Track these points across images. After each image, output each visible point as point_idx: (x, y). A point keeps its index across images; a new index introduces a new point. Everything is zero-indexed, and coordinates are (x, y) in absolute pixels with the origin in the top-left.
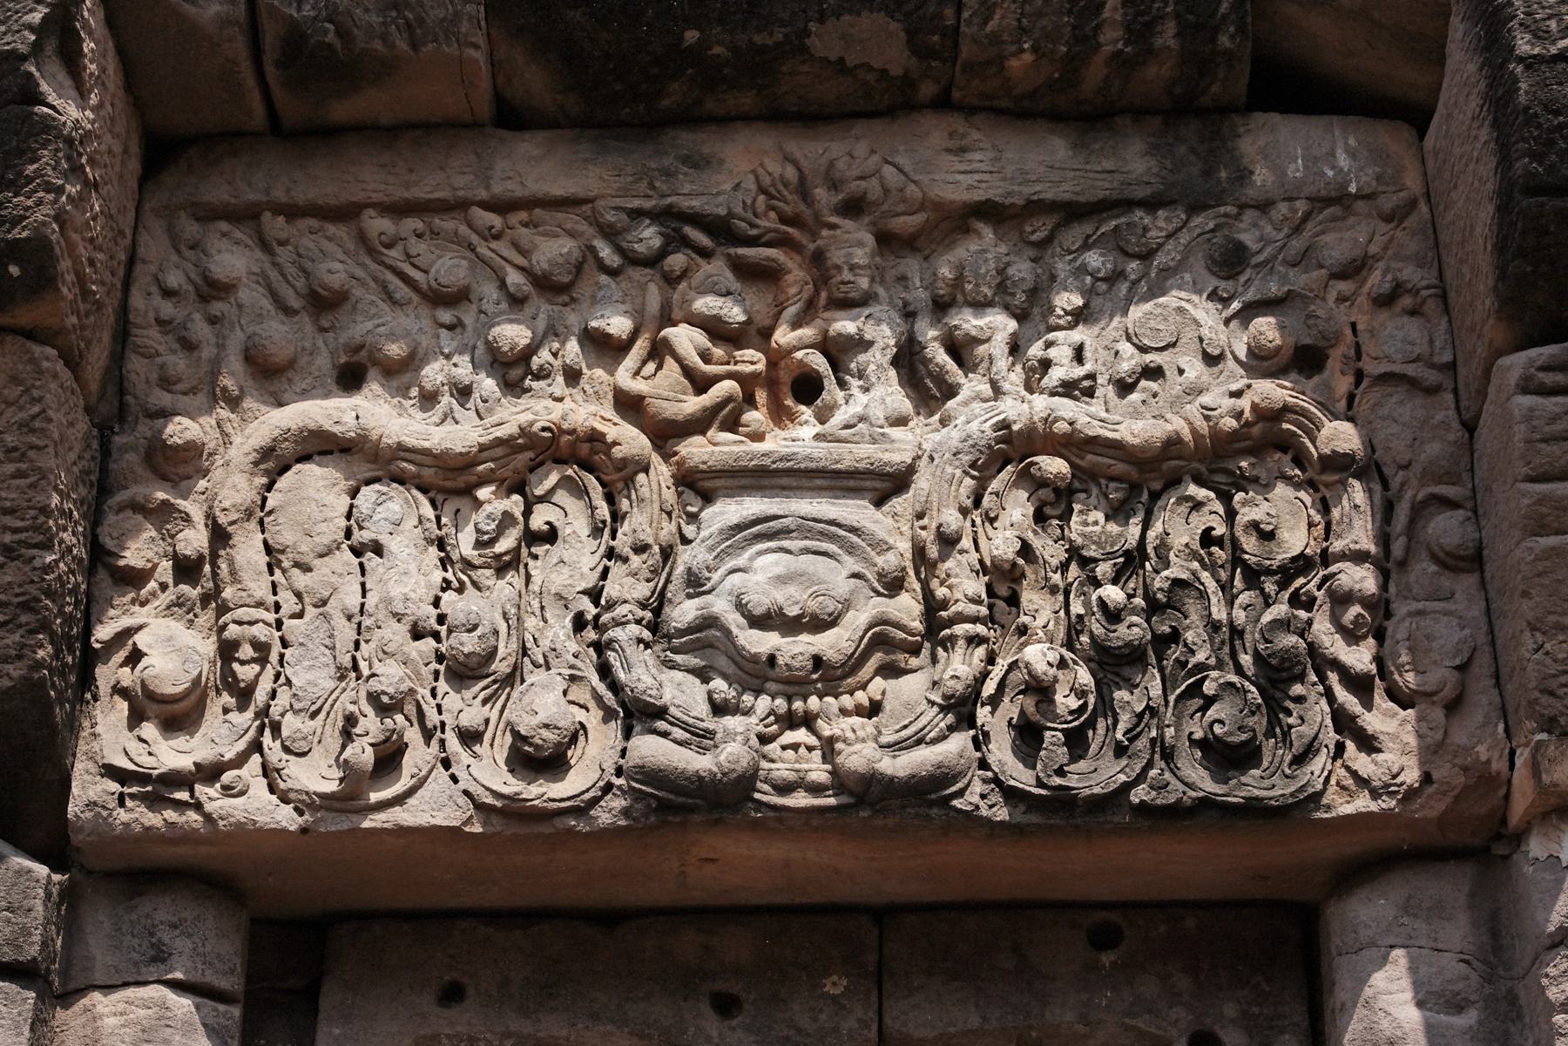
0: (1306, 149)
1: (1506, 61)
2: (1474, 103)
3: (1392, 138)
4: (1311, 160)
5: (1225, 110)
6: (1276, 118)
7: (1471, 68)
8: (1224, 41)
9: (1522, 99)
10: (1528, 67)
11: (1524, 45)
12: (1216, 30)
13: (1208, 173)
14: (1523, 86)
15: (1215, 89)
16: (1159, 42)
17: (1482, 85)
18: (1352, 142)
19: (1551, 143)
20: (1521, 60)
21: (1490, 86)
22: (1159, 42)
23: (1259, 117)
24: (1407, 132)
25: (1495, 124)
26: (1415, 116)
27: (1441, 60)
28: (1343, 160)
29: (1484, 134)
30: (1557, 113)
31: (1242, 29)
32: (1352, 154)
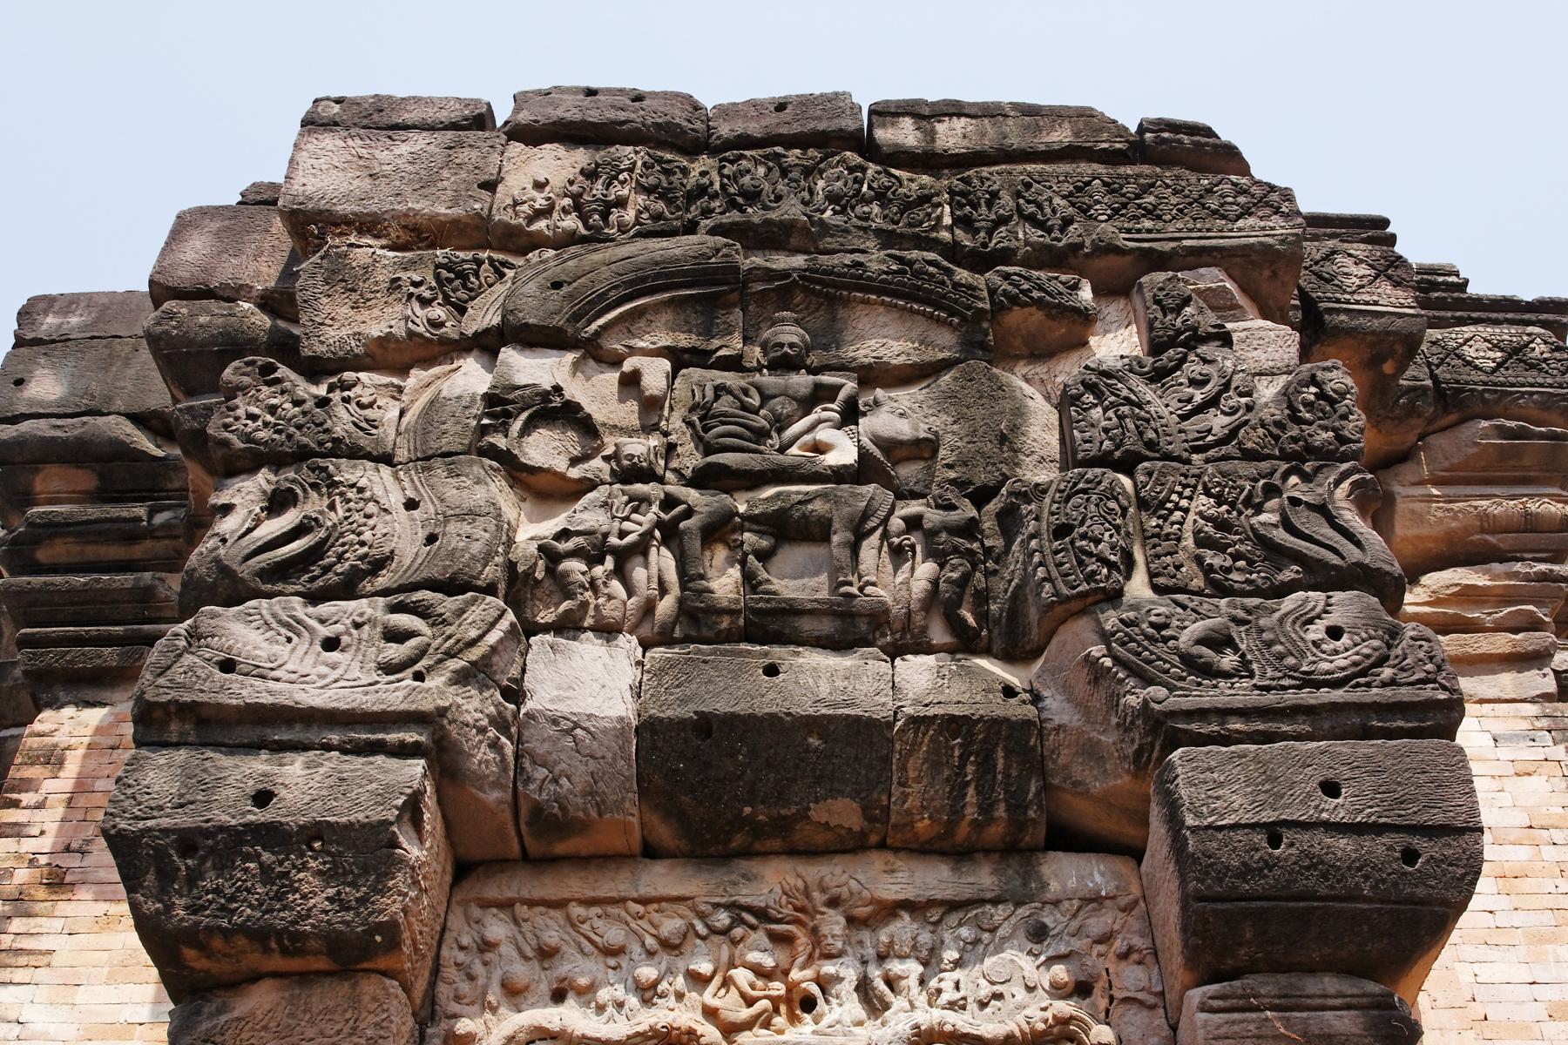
2: (1165, 850)
3: (1121, 865)
4: (1080, 878)
5: (1033, 850)
6: (1060, 854)
7: (1163, 831)
8: (1031, 813)
11: (1190, 820)
12: (1027, 808)
13: (1025, 885)
15: (1027, 838)
16: (996, 814)
19: (1208, 873)
22: (996, 814)
23: (1052, 854)
24: (1133, 863)
25: (1177, 862)
26: (1136, 853)
27: (1148, 825)
28: (1098, 878)
29: (1172, 867)
31: (1040, 807)
32: (1102, 875)
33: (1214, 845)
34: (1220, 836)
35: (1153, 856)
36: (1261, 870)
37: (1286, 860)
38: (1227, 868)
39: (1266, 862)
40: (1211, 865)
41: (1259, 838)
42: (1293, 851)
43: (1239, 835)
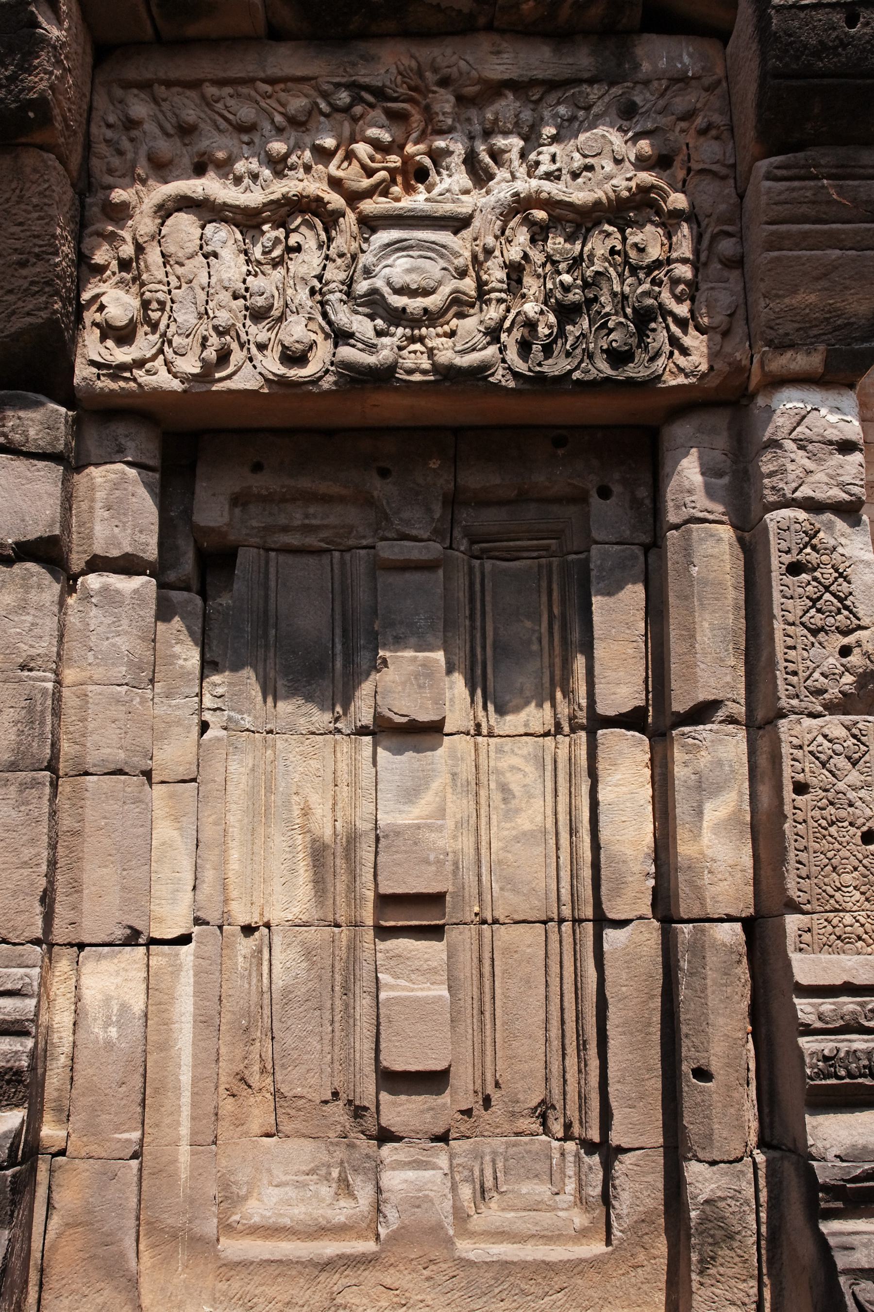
0: (668, 53)
1: (767, 8)
2: (750, 29)
3: (710, 47)
4: (670, 59)
7: (750, 11)
9: (774, 27)
10: (777, 11)
14: (774, 21)
15: (624, 21)
17: (755, 20)
18: (691, 49)
20: (774, 7)
21: (758, 21)
23: (646, 36)
25: (760, 41)
26: (722, 36)
28: (686, 59)
29: (754, 46)
30: (790, 36)
32: (690, 56)
33: (796, 24)
34: (802, 15)
35: (739, 36)
36: (835, 48)
37: (860, 39)
38: (805, 47)
39: (841, 40)
40: (792, 43)
41: (838, 18)
42: (867, 30)
43: (820, 15)
